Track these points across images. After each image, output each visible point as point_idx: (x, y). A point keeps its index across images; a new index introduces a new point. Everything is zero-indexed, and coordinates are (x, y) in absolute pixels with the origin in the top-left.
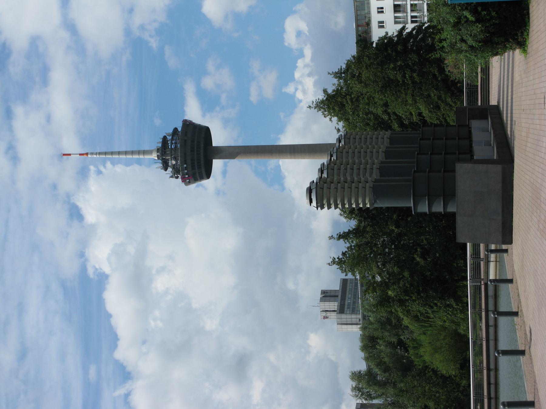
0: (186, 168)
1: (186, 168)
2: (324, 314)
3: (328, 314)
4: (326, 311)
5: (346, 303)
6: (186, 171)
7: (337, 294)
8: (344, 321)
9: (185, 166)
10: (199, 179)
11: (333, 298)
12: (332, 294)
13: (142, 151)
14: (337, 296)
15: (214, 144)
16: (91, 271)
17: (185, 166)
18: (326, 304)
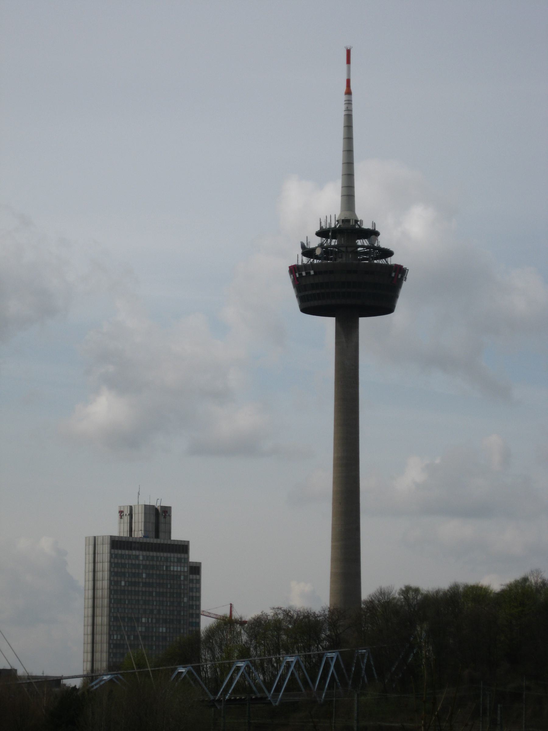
0: (308, 273)
1: (308, 273)
2: (127, 512)
3: (126, 519)
4: (131, 515)
5: (134, 553)
6: (304, 274)
7: (161, 535)
8: (99, 549)
9: (312, 272)
10: (198, 585)
11: (152, 528)
12: (162, 527)
13: (351, 107)
14: (157, 536)
15: (362, 321)
16: (233, 618)
17: (312, 272)
18: (140, 515)
